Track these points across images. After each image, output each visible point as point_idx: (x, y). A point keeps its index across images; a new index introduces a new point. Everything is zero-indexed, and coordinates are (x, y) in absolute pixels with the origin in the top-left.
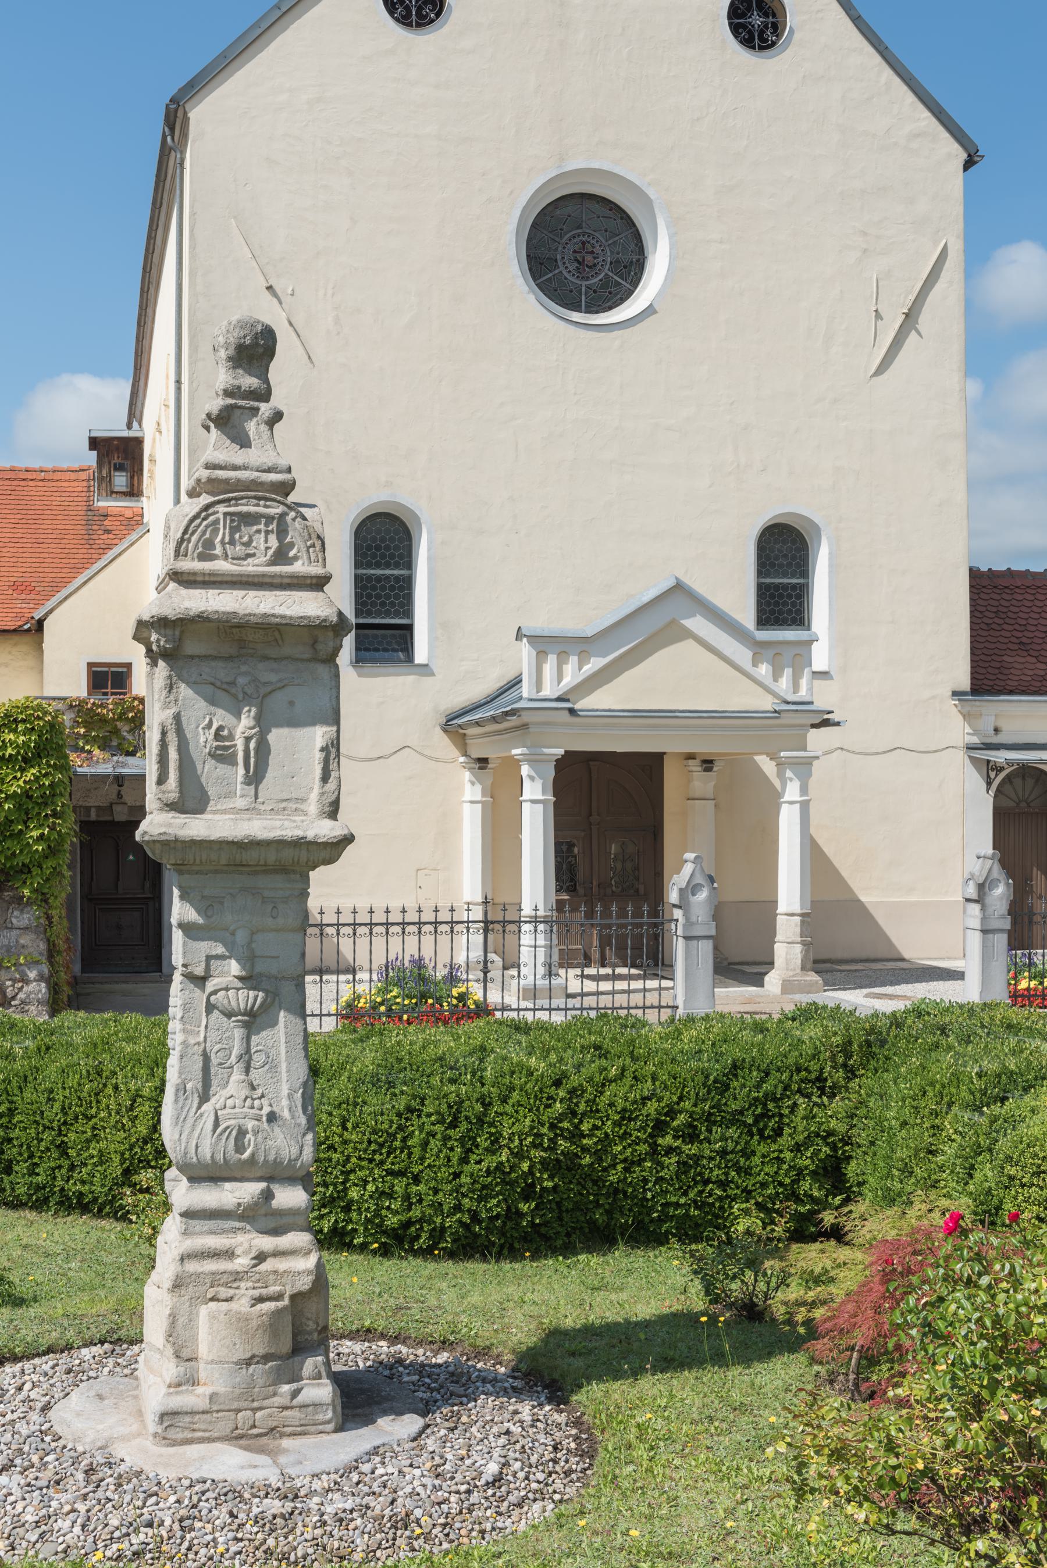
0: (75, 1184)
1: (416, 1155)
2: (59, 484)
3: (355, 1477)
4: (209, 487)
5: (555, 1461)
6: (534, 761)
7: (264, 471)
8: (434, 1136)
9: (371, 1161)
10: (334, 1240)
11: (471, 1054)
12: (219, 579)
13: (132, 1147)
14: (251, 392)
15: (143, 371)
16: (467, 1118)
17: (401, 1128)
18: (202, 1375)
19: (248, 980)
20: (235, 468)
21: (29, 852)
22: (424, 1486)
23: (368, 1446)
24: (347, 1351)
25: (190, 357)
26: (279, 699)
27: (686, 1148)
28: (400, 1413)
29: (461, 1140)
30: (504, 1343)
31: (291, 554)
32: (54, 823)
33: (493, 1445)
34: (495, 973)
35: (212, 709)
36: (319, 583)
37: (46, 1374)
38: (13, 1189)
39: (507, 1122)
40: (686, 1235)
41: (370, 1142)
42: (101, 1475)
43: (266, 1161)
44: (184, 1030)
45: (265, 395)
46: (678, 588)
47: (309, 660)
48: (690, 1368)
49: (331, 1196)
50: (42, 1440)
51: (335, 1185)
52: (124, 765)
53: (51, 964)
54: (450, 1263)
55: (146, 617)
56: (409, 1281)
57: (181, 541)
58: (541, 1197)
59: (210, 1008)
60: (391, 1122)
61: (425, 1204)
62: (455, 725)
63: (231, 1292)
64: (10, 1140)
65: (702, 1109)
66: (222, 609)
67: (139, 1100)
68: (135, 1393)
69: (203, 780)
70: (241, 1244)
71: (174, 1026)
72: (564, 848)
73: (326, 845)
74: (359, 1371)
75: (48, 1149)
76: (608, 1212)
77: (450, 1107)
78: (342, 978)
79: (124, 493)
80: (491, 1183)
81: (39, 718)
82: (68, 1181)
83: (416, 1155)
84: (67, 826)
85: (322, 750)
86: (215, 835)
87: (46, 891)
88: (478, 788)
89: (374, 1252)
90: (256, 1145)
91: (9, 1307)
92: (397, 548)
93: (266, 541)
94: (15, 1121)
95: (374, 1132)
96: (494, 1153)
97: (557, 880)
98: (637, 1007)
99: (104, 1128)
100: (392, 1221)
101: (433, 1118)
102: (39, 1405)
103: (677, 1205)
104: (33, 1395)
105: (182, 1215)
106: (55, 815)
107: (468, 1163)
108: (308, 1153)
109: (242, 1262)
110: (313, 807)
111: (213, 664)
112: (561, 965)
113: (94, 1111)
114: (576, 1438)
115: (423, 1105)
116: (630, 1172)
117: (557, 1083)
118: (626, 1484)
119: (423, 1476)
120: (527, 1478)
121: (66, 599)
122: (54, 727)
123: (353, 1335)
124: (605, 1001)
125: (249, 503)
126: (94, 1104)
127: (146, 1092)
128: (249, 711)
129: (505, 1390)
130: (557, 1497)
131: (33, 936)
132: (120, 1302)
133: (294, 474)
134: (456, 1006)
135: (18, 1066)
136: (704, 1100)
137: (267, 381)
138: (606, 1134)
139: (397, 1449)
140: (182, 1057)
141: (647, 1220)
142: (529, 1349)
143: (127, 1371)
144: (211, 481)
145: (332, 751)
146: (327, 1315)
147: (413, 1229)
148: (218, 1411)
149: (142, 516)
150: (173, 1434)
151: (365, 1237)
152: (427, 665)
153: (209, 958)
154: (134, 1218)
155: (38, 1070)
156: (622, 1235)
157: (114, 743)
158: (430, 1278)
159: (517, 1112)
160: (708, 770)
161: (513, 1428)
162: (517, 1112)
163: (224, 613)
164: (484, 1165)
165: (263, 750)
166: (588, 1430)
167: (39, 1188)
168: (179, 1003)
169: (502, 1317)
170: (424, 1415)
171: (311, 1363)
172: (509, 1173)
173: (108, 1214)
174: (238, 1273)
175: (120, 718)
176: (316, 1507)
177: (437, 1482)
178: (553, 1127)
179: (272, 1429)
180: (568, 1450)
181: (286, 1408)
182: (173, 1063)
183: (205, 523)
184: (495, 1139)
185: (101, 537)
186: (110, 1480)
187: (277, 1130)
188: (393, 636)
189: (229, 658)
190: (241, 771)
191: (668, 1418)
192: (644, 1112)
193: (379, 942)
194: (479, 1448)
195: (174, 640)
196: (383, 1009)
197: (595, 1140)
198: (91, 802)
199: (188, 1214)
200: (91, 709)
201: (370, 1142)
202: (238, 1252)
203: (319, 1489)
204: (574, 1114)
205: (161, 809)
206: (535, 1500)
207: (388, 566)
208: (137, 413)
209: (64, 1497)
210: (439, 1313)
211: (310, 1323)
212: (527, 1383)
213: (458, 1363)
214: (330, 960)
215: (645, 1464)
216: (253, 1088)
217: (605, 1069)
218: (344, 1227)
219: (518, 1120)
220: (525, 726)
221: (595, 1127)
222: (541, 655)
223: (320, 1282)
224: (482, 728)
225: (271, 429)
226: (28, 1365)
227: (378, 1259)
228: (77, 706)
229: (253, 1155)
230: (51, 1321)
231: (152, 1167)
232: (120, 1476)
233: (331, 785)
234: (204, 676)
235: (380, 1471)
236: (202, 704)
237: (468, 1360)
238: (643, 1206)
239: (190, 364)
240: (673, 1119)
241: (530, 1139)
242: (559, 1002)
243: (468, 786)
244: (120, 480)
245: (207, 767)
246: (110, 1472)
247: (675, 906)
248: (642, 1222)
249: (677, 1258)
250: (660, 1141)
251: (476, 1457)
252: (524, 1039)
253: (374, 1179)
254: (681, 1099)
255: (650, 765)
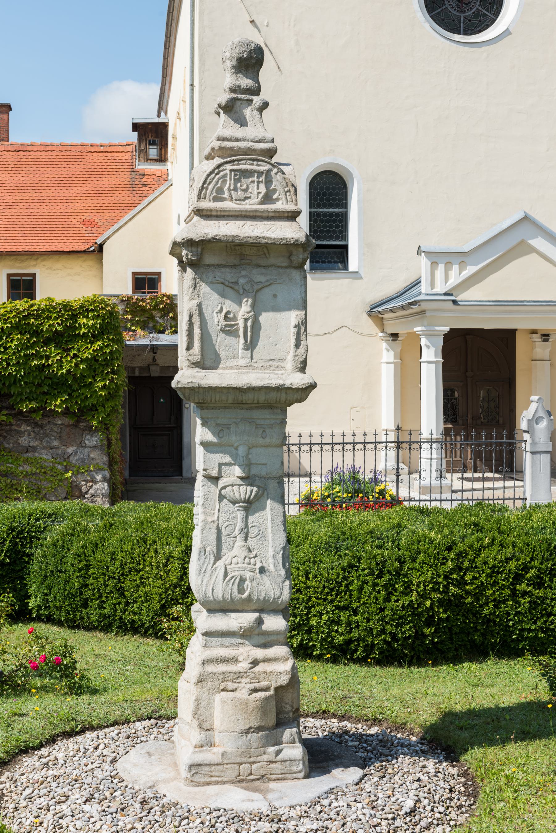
0: (129, 614)
1: (355, 596)
2: (113, 154)
3: (318, 808)
4: (220, 153)
5: (451, 799)
6: (429, 335)
7: (256, 142)
8: (367, 583)
9: (325, 600)
10: (302, 652)
11: (391, 529)
12: (227, 214)
13: (167, 590)
14: (248, 89)
15: (168, 78)
16: (389, 572)
17: (345, 578)
18: (217, 740)
19: (247, 479)
20: (237, 140)
21: (96, 396)
22: (364, 814)
23: (326, 788)
24: (311, 725)
25: (200, 69)
26: (267, 294)
27: (535, 592)
28: (347, 767)
29: (385, 586)
30: (415, 721)
31: (275, 197)
32: (112, 377)
33: (409, 788)
34: (404, 476)
35: (223, 300)
36: (293, 216)
37: (113, 739)
38: (89, 618)
39: (415, 574)
40: (536, 650)
41: (324, 587)
42: (151, 805)
43: (258, 599)
44: (204, 513)
45: (257, 91)
46: (526, 218)
47: (286, 267)
48: (540, 739)
49: (299, 623)
50: (112, 782)
51: (301, 616)
52: (157, 339)
53: (111, 470)
54: (378, 668)
55: (179, 240)
56: (350, 679)
57: (202, 188)
58: (438, 624)
59: (221, 498)
60: (338, 574)
61: (361, 628)
62: (376, 313)
63: (235, 685)
64: (86, 586)
65: (547, 566)
66: (229, 234)
67: (171, 559)
68: (172, 751)
69: (217, 347)
70: (242, 654)
71: (197, 510)
72: (449, 393)
73: (298, 389)
74: (319, 739)
75: (112, 592)
76: (483, 635)
77: (377, 564)
78: (303, 480)
79: (155, 160)
80: (405, 615)
81: (102, 308)
82: (124, 613)
83: (355, 596)
84: (121, 379)
85: (296, 326)
86: (225, 383)
87: (107, 422)
88: (392, 353)
89: (327, 661)
90: (252, 588)
91: (88, 695)
92: (337, 194)
93: (258, 188)
94: (90, 573)
95: (327, 581)
96: (407, 595)
97: (444, 414)
98: (499, 499)
99: (148, 578)
100: (339, 640)
101: (366, 572)
102: (109, 759)
103: (530, 630)
104: (105, 752)
105: (203, 635)
106: (113, 372)
107: (389, 601)
108: (286, 595)
109: (243, 666)
110: (289, 364)
111: (223, 270)
112: (448, 472)
113: (141, 566)
114: (465, 784)
115: (360, 563)
116: (498, 608)
117: (449, 549)
118: (499, 815)
119: (363, 808)
120: (432, 810)
121: (118, 230)
122: (112, 314)
123: (314, 715)
124: (478, 495)
125: (254, 161)
126: (142, 562)
127: (176, 554)
128: (247, 301)
129: (416, 751)
130: (452, 823)
131: (99, 452)
132: (160, 692)
133: (276, 143)
134: (378, 498)
135: (91, 537)
136: (548, 560)
137: (258, 82)
138: (482, 582)
139: (346, 790)
140: (203, 530)
141: (509, 640)
142: (432, 725)
143: (166, 737)
144: (221, 148)
145: (302, 327)
146: (299, 700)
147: (353, 645)
148: (227, 764)
149: (167, 175)
150: (197, 778)
151: (321, 650)
152: (357, 272)
153: (220, 465)
154: (169, 637)
155: (105, 539)
156: (493, 650)
157: (151, 325)
158: (364, 677)
159: (422, 567)
160: (546, 340)
161: (422, 777)
162: (422, 567)
163: (230, 236)
164: (400, 603)
165: (256, 326)
166: (472, 779)
167: (105, 617)
168: (201, 494)
169: (413, 704)
170: (363, 768)
171: (288, 733)
172: (417, 608)
173: (151, 634)
174: (240, 672)
175: (154, 309)
176: (294, 828)
177: (373, 812)
178: (446, 577)
179: (263, 776)
180: (459, 792)
181: (272, 762)
182: (197, 535)
183: (217, 177)
184: (408, 586)
185: (141, 190)
186: (157, 808)
187: (266, 578)
188: (335, 253)
189: (234, 266)
190: (242, 340)
191: (526, 772)
192: (508, 568)
193: (327, 456)
194: (400, 790)
195: (197, 255)
196: (329, 500)
197: (475, 586)
198: (136, 364)
199: (207, 634)
200: (136, 302)
201: (324, 587)
202: (240, 659)
203: (295, 816)
204: (460, 569)
205: (189, 367)
206: (438, 825)
207: (331, 206)
208: (164, 107)
209: (127, 819)
210: (371, 700)
211: (288, 706)
212: (431, 748)
213: (384, 734)
214: (294, 468)
215: (511, 802)
216: (250, 551)
217: (481, 539)
218: (307, 644)
219: (423, 573)
220: (423, 312)
221: (474, 578)
222: (434, 264)
223: (294, 680)
224: (392, 314)
225: (261, 113)
226: (101, 733)
227: (330, 665)
228: (126, 301)
229: (250, 595)
230: (116, 703)
231: (180, 604)
232: (163, 806)
233: (302, 350)
234: (217, 278)
235: (335, 804)
236: (215, 297)
237: (391, 732)
238: (506, 631)
239: (200, 73)
240: (527, 573)
241: (431, 586)
242: (447, 496)
243: (385, 352)
244: (153, 151)
245: (219, 338)
246: (157, 803)
247: (524, 431)
248: (505, 641)
249: (531, 666)
250: (518, 587)
251: (398, 796)
252: (426, 519)
253: (327, 612)
254: (532, 559)
255: (505, 339)
